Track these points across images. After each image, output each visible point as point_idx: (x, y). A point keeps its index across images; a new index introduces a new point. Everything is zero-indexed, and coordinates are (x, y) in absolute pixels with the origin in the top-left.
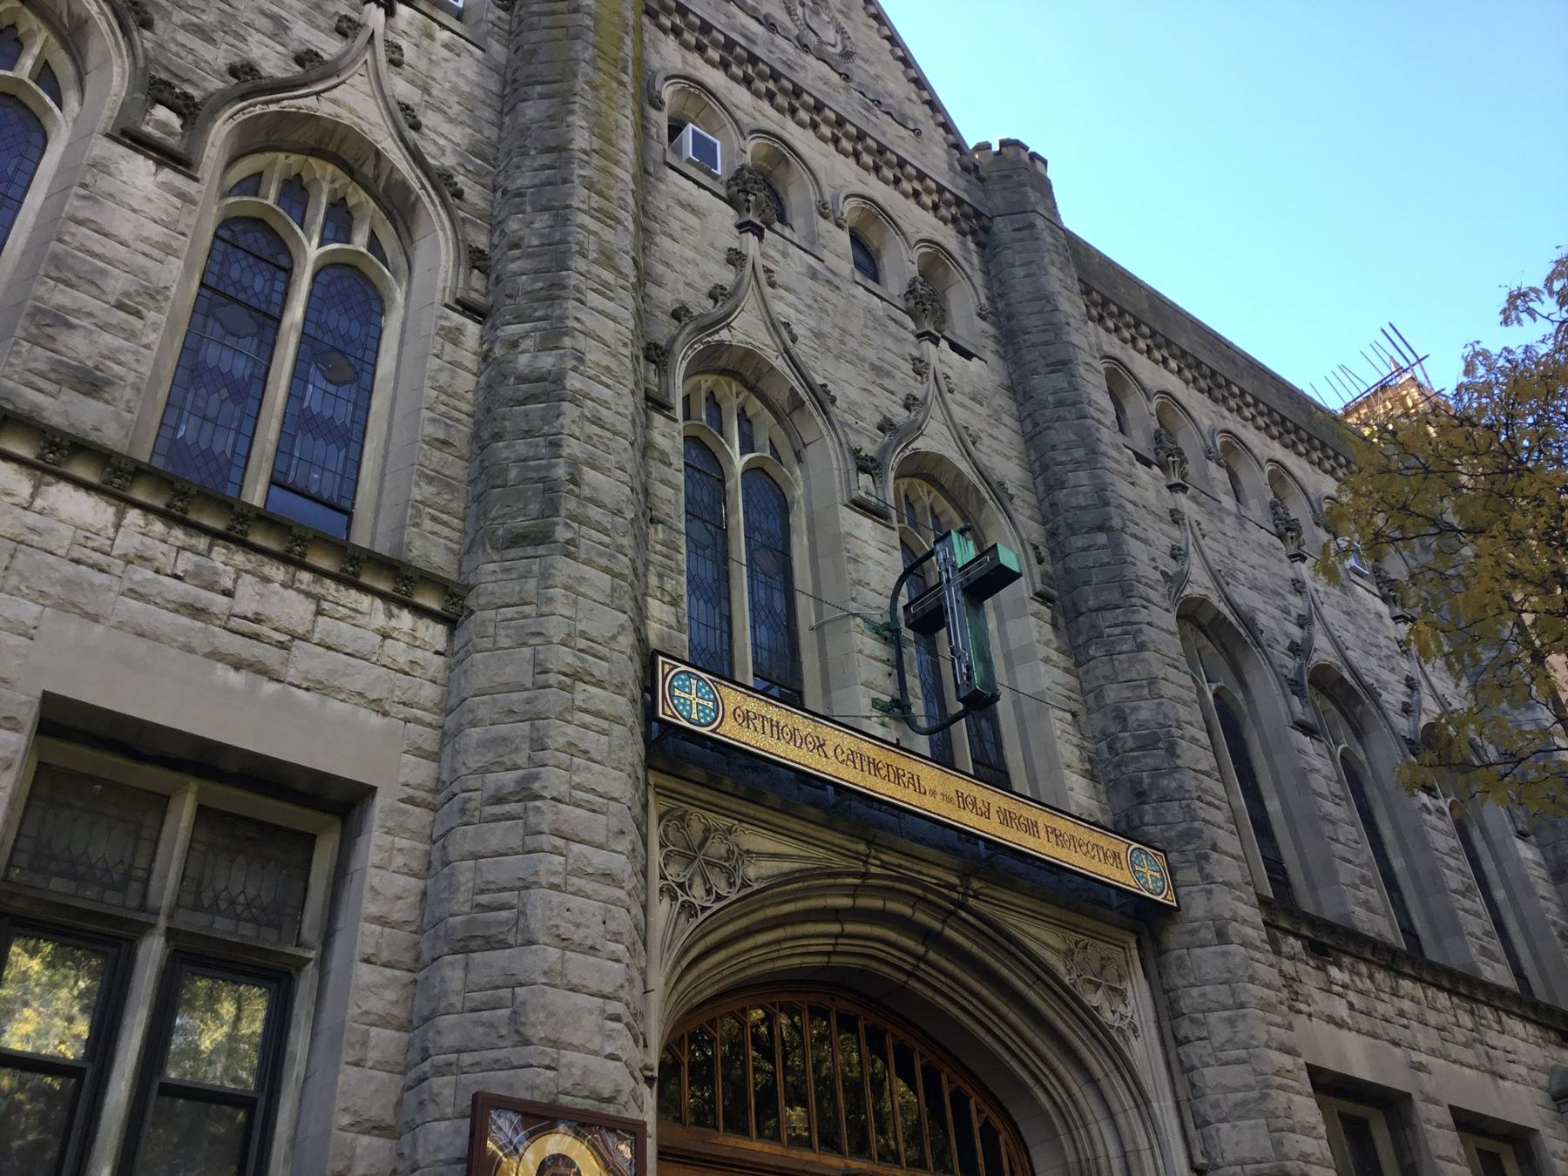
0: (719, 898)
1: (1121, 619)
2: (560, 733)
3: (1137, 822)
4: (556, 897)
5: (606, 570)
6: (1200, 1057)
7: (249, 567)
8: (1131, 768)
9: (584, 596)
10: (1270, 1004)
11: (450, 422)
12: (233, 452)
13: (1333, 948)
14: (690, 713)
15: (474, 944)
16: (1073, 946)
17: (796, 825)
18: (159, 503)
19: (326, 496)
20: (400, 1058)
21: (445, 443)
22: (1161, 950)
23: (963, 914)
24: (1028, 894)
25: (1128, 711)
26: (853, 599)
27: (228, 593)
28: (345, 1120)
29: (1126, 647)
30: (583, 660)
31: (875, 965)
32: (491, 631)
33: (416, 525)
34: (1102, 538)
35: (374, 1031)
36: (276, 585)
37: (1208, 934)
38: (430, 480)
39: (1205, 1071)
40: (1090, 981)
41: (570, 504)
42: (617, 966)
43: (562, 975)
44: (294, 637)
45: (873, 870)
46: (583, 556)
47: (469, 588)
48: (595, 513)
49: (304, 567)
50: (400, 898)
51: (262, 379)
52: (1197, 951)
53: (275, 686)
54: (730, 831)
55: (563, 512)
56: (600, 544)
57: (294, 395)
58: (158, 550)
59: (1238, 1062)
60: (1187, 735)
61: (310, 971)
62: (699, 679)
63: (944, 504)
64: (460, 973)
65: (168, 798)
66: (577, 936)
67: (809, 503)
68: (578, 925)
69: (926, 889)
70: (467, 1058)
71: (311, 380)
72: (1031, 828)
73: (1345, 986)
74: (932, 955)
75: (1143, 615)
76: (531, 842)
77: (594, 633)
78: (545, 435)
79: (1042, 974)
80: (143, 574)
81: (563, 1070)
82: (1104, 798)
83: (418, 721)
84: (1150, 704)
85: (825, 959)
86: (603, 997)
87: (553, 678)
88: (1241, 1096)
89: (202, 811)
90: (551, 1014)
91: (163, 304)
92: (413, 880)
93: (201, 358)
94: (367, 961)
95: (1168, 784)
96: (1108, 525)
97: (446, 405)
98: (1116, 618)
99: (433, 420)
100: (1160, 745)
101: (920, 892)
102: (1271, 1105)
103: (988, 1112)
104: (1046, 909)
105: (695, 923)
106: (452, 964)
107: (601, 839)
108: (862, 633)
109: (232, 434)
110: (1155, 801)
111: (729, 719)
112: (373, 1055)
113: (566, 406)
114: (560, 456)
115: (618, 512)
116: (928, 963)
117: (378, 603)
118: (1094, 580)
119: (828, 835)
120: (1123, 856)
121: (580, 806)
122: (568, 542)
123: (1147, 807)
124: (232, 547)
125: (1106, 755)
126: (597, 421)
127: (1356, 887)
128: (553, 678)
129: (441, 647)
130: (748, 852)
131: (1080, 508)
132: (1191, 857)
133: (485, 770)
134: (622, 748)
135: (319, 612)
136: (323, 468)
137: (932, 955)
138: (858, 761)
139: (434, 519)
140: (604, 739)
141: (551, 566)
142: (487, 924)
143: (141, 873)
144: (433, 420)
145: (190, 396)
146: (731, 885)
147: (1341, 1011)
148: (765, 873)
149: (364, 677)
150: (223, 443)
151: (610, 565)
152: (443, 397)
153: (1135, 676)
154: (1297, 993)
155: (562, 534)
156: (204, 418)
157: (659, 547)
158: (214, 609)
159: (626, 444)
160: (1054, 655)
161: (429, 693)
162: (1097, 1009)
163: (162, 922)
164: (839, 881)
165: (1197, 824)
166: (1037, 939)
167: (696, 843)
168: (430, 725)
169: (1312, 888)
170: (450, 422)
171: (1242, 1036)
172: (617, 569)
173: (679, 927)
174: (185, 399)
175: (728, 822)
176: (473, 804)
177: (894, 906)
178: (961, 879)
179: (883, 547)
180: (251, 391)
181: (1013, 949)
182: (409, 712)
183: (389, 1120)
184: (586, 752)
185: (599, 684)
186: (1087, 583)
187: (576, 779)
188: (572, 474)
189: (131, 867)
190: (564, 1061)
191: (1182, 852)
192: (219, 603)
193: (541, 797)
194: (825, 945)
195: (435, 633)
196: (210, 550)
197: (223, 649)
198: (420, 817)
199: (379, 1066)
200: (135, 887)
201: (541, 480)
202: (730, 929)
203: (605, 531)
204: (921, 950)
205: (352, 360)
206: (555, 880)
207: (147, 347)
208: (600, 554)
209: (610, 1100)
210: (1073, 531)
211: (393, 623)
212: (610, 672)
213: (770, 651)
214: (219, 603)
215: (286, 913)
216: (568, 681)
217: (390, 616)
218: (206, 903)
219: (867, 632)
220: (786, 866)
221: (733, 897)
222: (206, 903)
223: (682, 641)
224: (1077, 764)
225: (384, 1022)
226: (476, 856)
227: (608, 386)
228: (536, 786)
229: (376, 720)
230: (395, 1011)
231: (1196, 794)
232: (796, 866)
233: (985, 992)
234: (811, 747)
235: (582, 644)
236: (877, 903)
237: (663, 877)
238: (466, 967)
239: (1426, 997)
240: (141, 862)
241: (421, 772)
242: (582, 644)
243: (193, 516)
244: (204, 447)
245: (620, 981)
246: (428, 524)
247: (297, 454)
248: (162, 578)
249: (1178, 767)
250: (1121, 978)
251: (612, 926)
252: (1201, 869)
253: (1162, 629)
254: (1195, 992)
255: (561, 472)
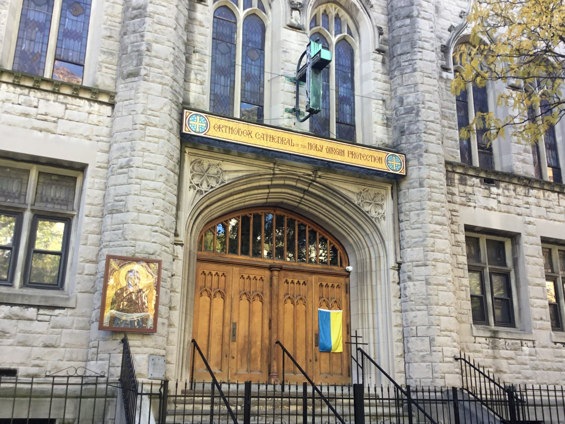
0: (212, 187)
1: (409, 58)
2: (140, 145)
3: (399, 143)
4: (136, 197)
5: (160, 83)
6: (405, 226)
7: (42, 97)
8: (401, 122)
9: (151, 94)
10: (436, 208)
11: (112, 28)
12: (42, 51)
13: (496, 180)
14: (196, 129)
15: (114, 212)
16: (362, 191)
17: (244, 160)
18: (11, 81)
19: (74, 61)
20: (98, 243)
21: (110, 37)
22: (399, 190)
23: (315, 183)
24: (343, 174)
25: (404, 98)
26: (282, 69)
27: (36, 107)
28: (81, 260)
29: (408, 71)
30: (149, 118)
31: (285, 201)
32: (121, 110)
33: (100, 71)
34: (408, 21)
35: (89, 235)
36: (52, 102)
37: (416, 184)
38: (104, 53)
39: (406, 231)
40: (367, 202)
41: (146, 60)
42: (157, 216)
43: (138, 220)
44: (58, 118)
45: (277, 172)
46: (151, 79)
47: (116, 93)
48: (156, 61)
49: (59, 93)
50: (96, 197)
51: (49, 20)
52: (411, 190)
53: (54, 135)
54: (218, 165)
55: (143, 63)
56: (159, 73)
57: (60, 24)
58: (12, 96)
59: (418, 228)
60: (427, 106)
61: (75, 217)
62: (201, 116)
63: (342, 13)
64: (110, 220)
65: (29, 171)
66: (143, 209)
67: (272, 27)
68: (144, 206)
69: (299, 176)
70: (111, 244)
71: (67, 16)
72: (342, 153)
73: (498, 195)
74: (306, 197)
75: (419, 56)
76: (130, 181)
77: (154, 108)
78: (140, 32)
79: (347, 201)
80: (8, 105)
81: (137, 247)
82: (391, 133)
83: (102, 141)
84: (413, 95)
85: (265, 200)
86: (152, 225)
87: (138, 126)
88: (416, 240)
89: (40, 173)
90: (133, 232)
91: (7, 6)
92: (101, 191)
93: (28, 18)
94: (87, 216)
95: (413, 127)
96: (411, 14)
97: (110, 21)
98: (407, 58)
99: (106, 29)
100: (414, 112)
101: (297, 178)
102: (426, 243)
103: (334, 243)
104: (351, 179)
105: (202, 196)
106: (108, 217)
107: (153, 178)
108: (285, 82)
109: (41, 44)
110: (408, 134)
111: (212, 129)
112: (89, 242)
113: (147, 19)
114: (144, 41)
115: (167, 59)
116: (305, 199)
117: (86, 102)
118: (402, 41)
119: (257, 162)
120: (383, 159)
121: (146, 168)
122: (145, 75)
123: (404, 137)
124: (36, 91)
125: (394, 116)
126: (159, 23)
127: (520, 154)
128: (138, 126)
129: (109, 114)
130: (225, 171)
131: (401, 7)
132: (416, 155)
133: (118, 158)
134: (163, 147)
135: (66, 109)
136: (73, 51)
137: (306, 197)
138: (265, 138)
139: (106, 67)
140: (156, 145)
141: (139, 85)
142: (117, 206)
143: (24, 194)
144: (106, 29)
145: (25, 33)
146: (217, 183)
147: (493, 203)
148: (232, 177)
149: (84, 129)
150: (37, 49)
151: (162, 81)
152: (110, 18)
153: (410, 83)
154: (470, 199)
155: (143, 72)
156: (31, 40)
157: (197, 62)
158: (31, 113)
159: (172, 30)
160: (379, 76)
161: (106, 131)
162: (368, 212)
163: (29, 207)
164: (263, 177)
165: (421, 143)
166: (346, 189)
167: (205, 169)
168: (106, 142)
169: (501, 155)
170: (112, 28)
171: (421, 220)
172: (164, 82)
173: (196, 198)
174: (24, 35)
175: (218, 162)
176: (114, 169)
177: (287, 182)
178: (313, 172)
179: (300, 43)
180: (45, 27)
181: (335, 193)
182: (98, 138)
183: (94, 259)
184: (149, 150)
185: (155, 126)
186: (398, 43)
187: (145, 160)
188: (147, 48)
189: (21, 192)
190: (137, 244)
191: (413, 154)
192: (33, 111)
193: (132, 167)
194: (265, 196)
195: (107, 110)
196: (29, 93)
197: (36, 126)
198: (103, 172)
199: (92, 245)
200: (22, 197)
201: (138, 51)
202: (220, 196)
203: (160, 68)
204: (302, 195)
205: (82, 5)
206: (136, 192)
207: (3, 24)
208: (158, 78)
209: (153, 254)
210: (397, 19)
211: (92, 108)
212: (159, 121)
213: (251, 92)
214: (33, 111)
215: (68, 201)
216: (143, 126)
217: (91, 106)
218: (44, 200)
219: (287, 81)
220: (240, 174)
221: (218, 187)
222: (44, 200)
223: (203, 98)
224: (380, 121)
225: (92, 233)
226: (115, 185)
227: (165, 6)
228: (131, 163)
229: (88, 142)
230: (96, 230)
231: (423, 131)
232: (245, 174)
233: (327, 208)
234: (245, 135)
235: (149, 112)
236: (282, 182)
237: (191, 183)
238: (112, 218)
239: (544, 196)
240: (24, 190)
241: (103, 157)
242: (149, 112)
243: (22, 83)
244: (31, 51)
245: (157, 221)
246: (104, 70)
247: (64, 47)
248: (14, 106)
249: (418, 120)
250: (382, 200)
251: (156, 205)
252: (419, 160)
253: (427, 61)
254: (408, 204)
255: (144, 48)
